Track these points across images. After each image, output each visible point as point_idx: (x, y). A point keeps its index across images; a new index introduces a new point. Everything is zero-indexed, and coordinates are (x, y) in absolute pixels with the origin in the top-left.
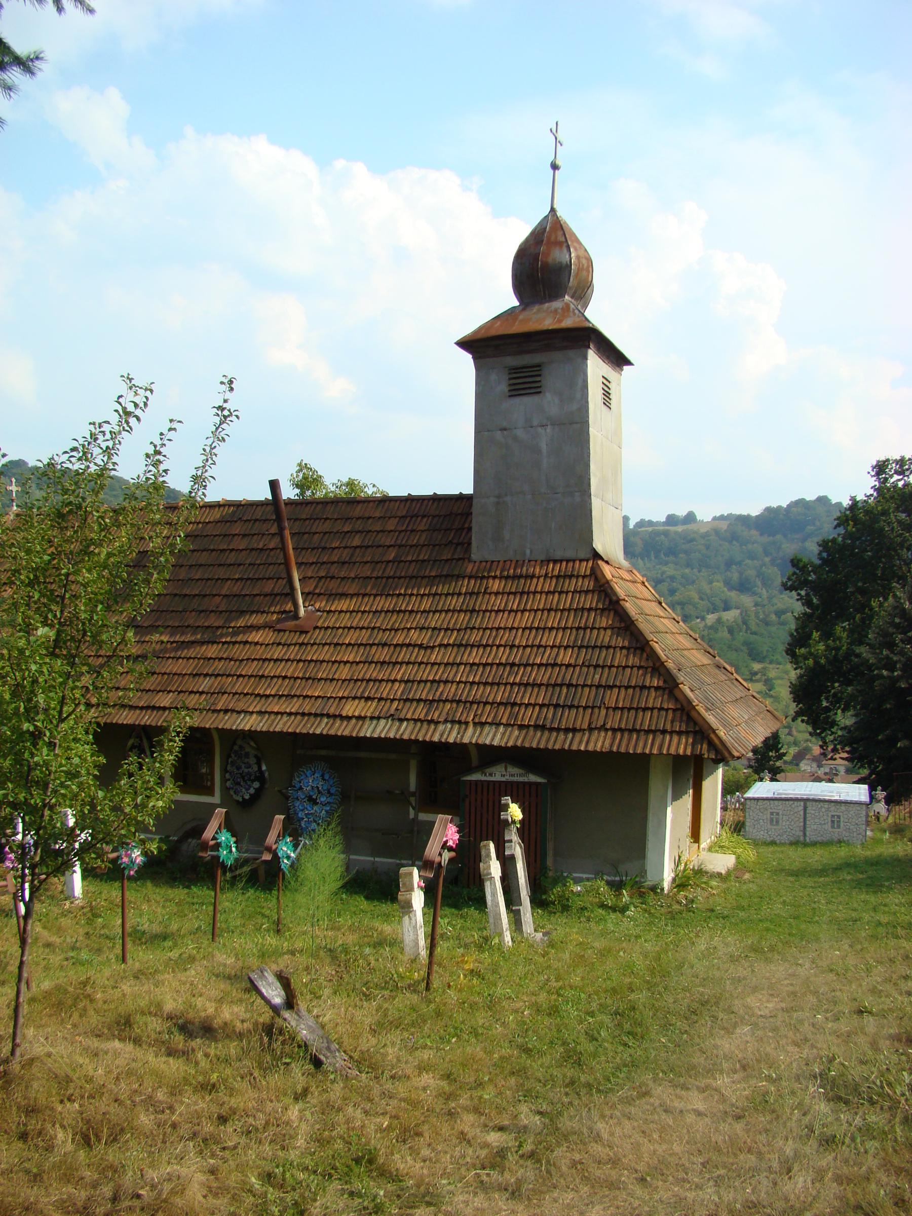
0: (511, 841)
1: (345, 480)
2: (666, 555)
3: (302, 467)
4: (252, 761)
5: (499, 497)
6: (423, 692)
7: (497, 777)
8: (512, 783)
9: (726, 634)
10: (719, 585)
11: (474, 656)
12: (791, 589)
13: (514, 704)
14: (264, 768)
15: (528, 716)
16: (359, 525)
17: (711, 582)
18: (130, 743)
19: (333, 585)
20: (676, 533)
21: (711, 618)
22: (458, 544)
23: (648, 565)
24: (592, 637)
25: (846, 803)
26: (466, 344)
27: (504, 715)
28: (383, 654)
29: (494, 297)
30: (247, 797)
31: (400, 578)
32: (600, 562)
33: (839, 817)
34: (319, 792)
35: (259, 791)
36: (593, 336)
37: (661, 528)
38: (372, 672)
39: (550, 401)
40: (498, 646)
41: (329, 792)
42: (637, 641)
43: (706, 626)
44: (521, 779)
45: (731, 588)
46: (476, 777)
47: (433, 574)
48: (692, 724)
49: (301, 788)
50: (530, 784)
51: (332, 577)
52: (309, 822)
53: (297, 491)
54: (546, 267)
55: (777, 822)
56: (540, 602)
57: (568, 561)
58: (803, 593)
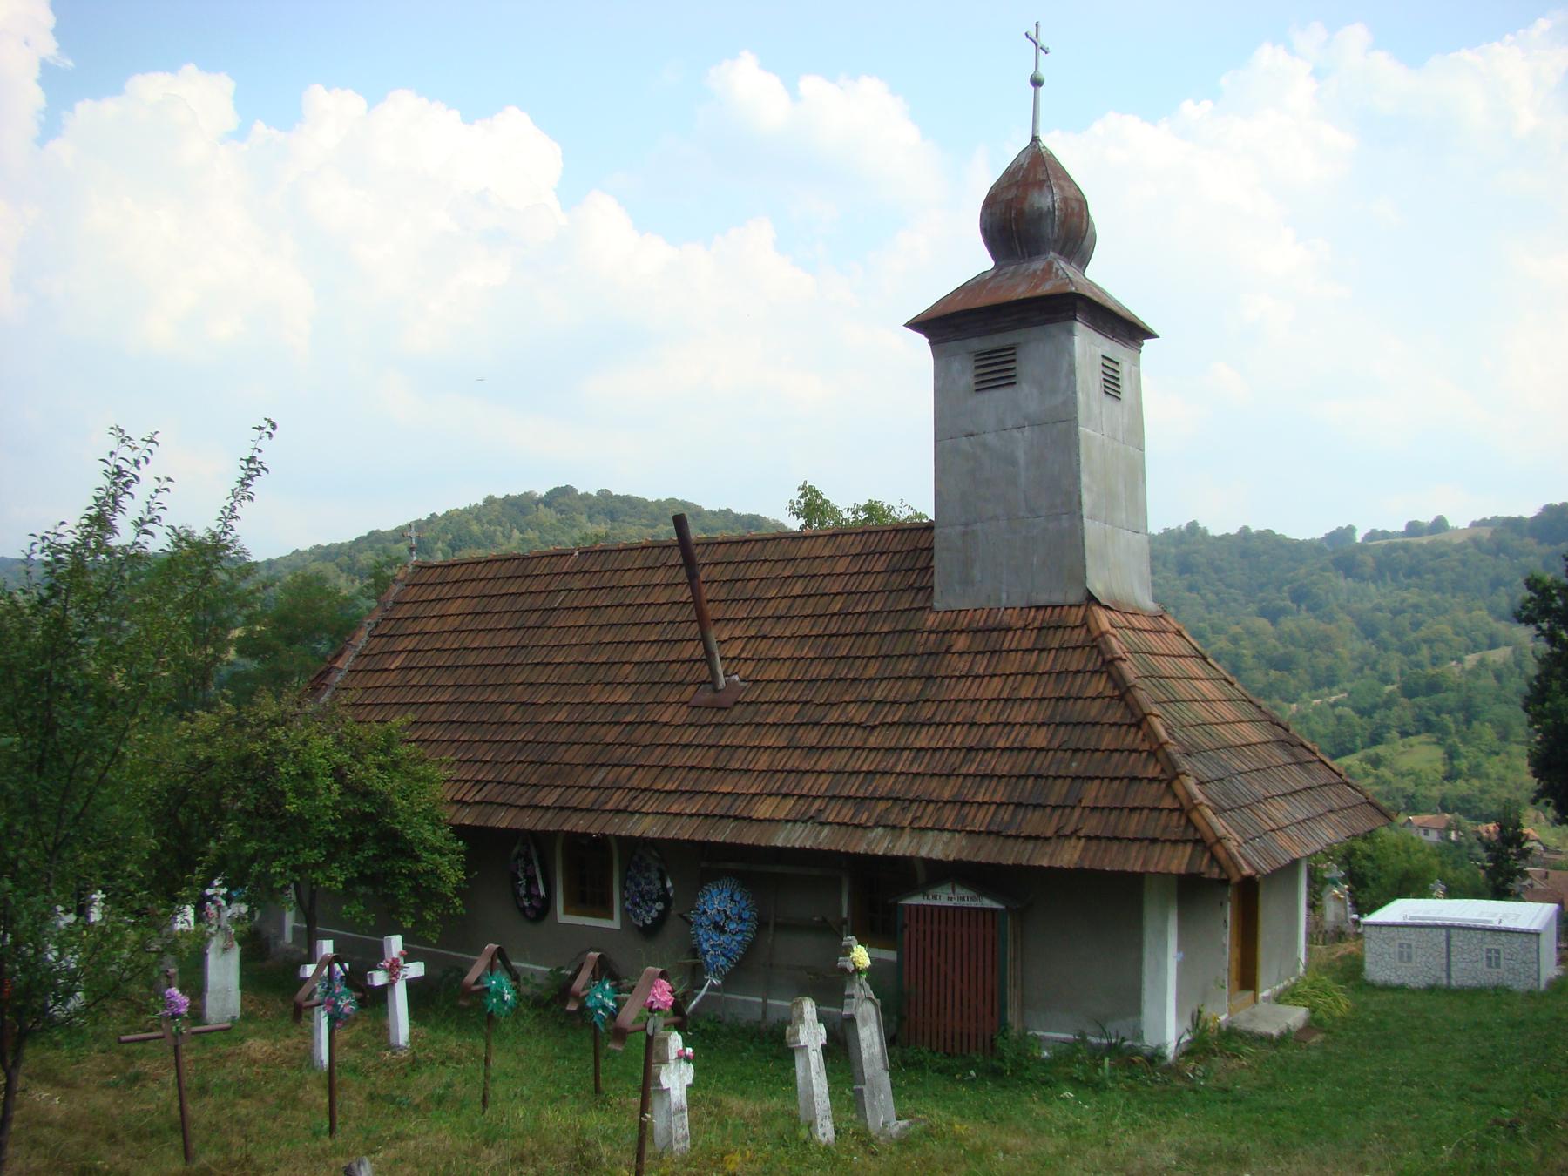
0: (852, 997)
1: (863, 503)
2: (1408, 575)
3: (808, 491)
4: (654, 875)
5: (966, 525)
6: (852, 788)
7: (943, 901)
8: (962, 908)
9: (1492, 682)
10: (1481, 614)
11: (923, 739)
12: (1528, 620)
13: (964, 803)
14: (669, 884)
15: (980, 819)
16: (803, 568)
17: (1469, 610)
18: (516, 849)
19: (763, 647)
20: (1420, 545)
21: (1471, 660)
22: (920, 589)
23: (1383, 591)
24: (1077, 710)
25: (1508, 931)
26: (917, 325)
27: (949, 816)
28: (811, 737)
29: (968, 259)
30: (649, 922)
31: (845, 635)
32: (1095, 608)
33: (1497, 951)
34: (727, 917)
35: (662, 917)
36: (1079, 304)
37: (1399, 540)
38: (795, 760)
39: (1026, 396)
40: (954, 725)
41: (740, 917)
42: (1133, 715)
43: (1463, 670)
44: (973, 904)
45: (1500, 618)
46: (917, 900)
47: (885, 629)
48: (1191, 830)
49: (705, 912)
50: (984, 910)
51: (764, 637)
52: (716, 956)
53: (802, 521)
54: (1032, 216)
55: (1409, 957)
56: (1013, 663)
57: (1054, 607)
58: (1545, 626)
